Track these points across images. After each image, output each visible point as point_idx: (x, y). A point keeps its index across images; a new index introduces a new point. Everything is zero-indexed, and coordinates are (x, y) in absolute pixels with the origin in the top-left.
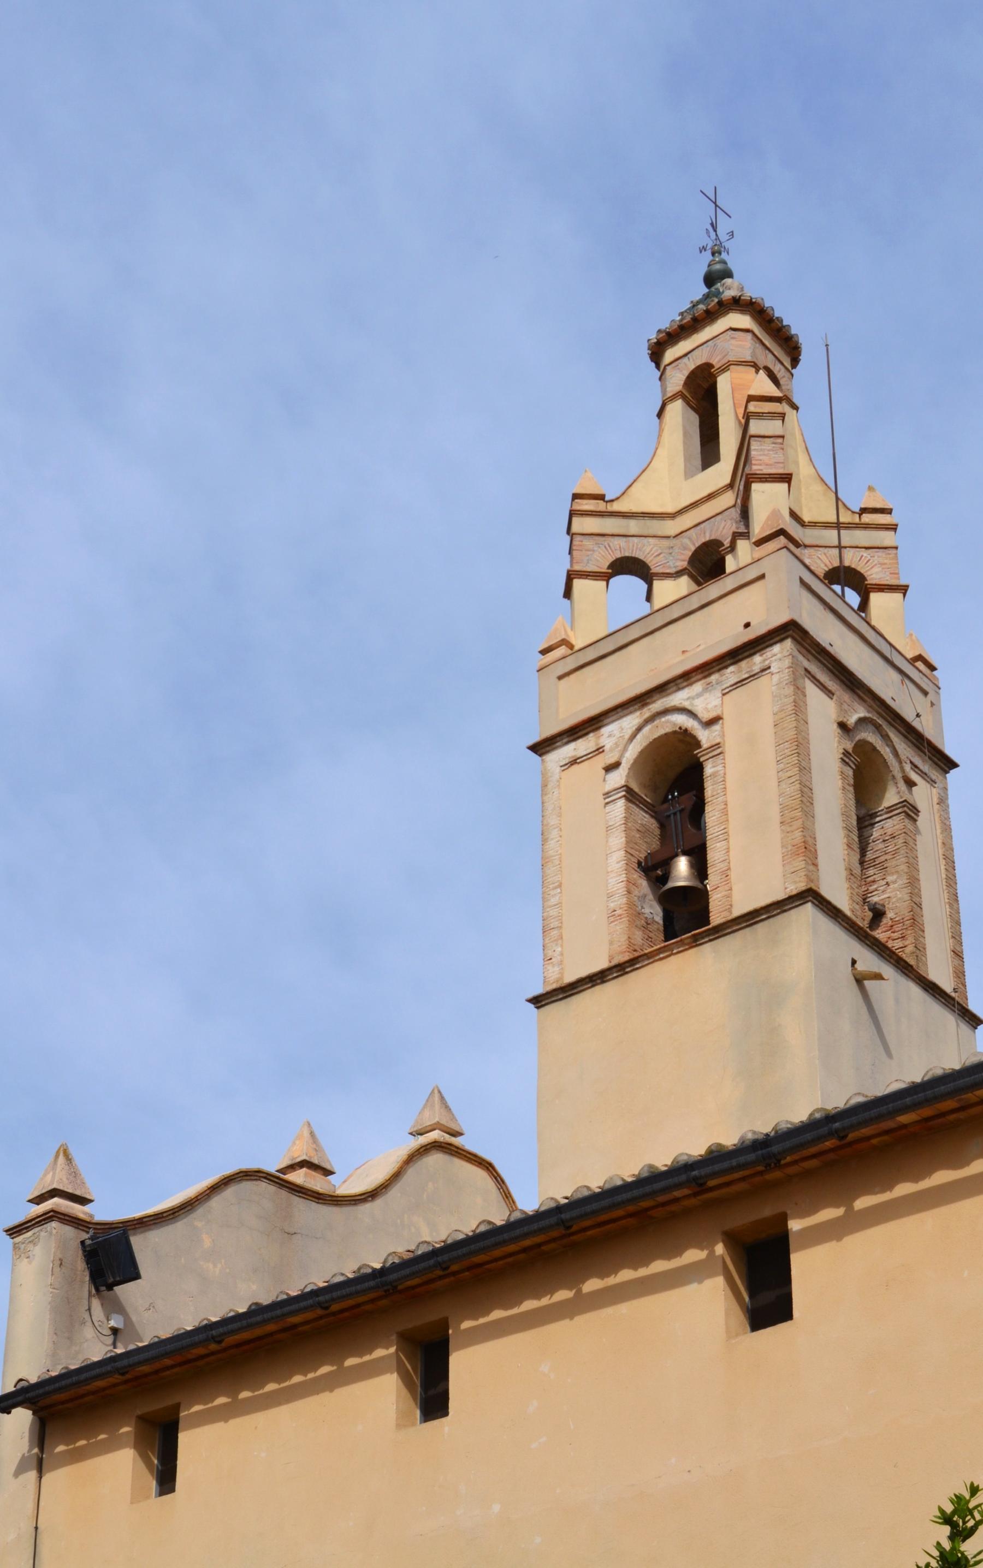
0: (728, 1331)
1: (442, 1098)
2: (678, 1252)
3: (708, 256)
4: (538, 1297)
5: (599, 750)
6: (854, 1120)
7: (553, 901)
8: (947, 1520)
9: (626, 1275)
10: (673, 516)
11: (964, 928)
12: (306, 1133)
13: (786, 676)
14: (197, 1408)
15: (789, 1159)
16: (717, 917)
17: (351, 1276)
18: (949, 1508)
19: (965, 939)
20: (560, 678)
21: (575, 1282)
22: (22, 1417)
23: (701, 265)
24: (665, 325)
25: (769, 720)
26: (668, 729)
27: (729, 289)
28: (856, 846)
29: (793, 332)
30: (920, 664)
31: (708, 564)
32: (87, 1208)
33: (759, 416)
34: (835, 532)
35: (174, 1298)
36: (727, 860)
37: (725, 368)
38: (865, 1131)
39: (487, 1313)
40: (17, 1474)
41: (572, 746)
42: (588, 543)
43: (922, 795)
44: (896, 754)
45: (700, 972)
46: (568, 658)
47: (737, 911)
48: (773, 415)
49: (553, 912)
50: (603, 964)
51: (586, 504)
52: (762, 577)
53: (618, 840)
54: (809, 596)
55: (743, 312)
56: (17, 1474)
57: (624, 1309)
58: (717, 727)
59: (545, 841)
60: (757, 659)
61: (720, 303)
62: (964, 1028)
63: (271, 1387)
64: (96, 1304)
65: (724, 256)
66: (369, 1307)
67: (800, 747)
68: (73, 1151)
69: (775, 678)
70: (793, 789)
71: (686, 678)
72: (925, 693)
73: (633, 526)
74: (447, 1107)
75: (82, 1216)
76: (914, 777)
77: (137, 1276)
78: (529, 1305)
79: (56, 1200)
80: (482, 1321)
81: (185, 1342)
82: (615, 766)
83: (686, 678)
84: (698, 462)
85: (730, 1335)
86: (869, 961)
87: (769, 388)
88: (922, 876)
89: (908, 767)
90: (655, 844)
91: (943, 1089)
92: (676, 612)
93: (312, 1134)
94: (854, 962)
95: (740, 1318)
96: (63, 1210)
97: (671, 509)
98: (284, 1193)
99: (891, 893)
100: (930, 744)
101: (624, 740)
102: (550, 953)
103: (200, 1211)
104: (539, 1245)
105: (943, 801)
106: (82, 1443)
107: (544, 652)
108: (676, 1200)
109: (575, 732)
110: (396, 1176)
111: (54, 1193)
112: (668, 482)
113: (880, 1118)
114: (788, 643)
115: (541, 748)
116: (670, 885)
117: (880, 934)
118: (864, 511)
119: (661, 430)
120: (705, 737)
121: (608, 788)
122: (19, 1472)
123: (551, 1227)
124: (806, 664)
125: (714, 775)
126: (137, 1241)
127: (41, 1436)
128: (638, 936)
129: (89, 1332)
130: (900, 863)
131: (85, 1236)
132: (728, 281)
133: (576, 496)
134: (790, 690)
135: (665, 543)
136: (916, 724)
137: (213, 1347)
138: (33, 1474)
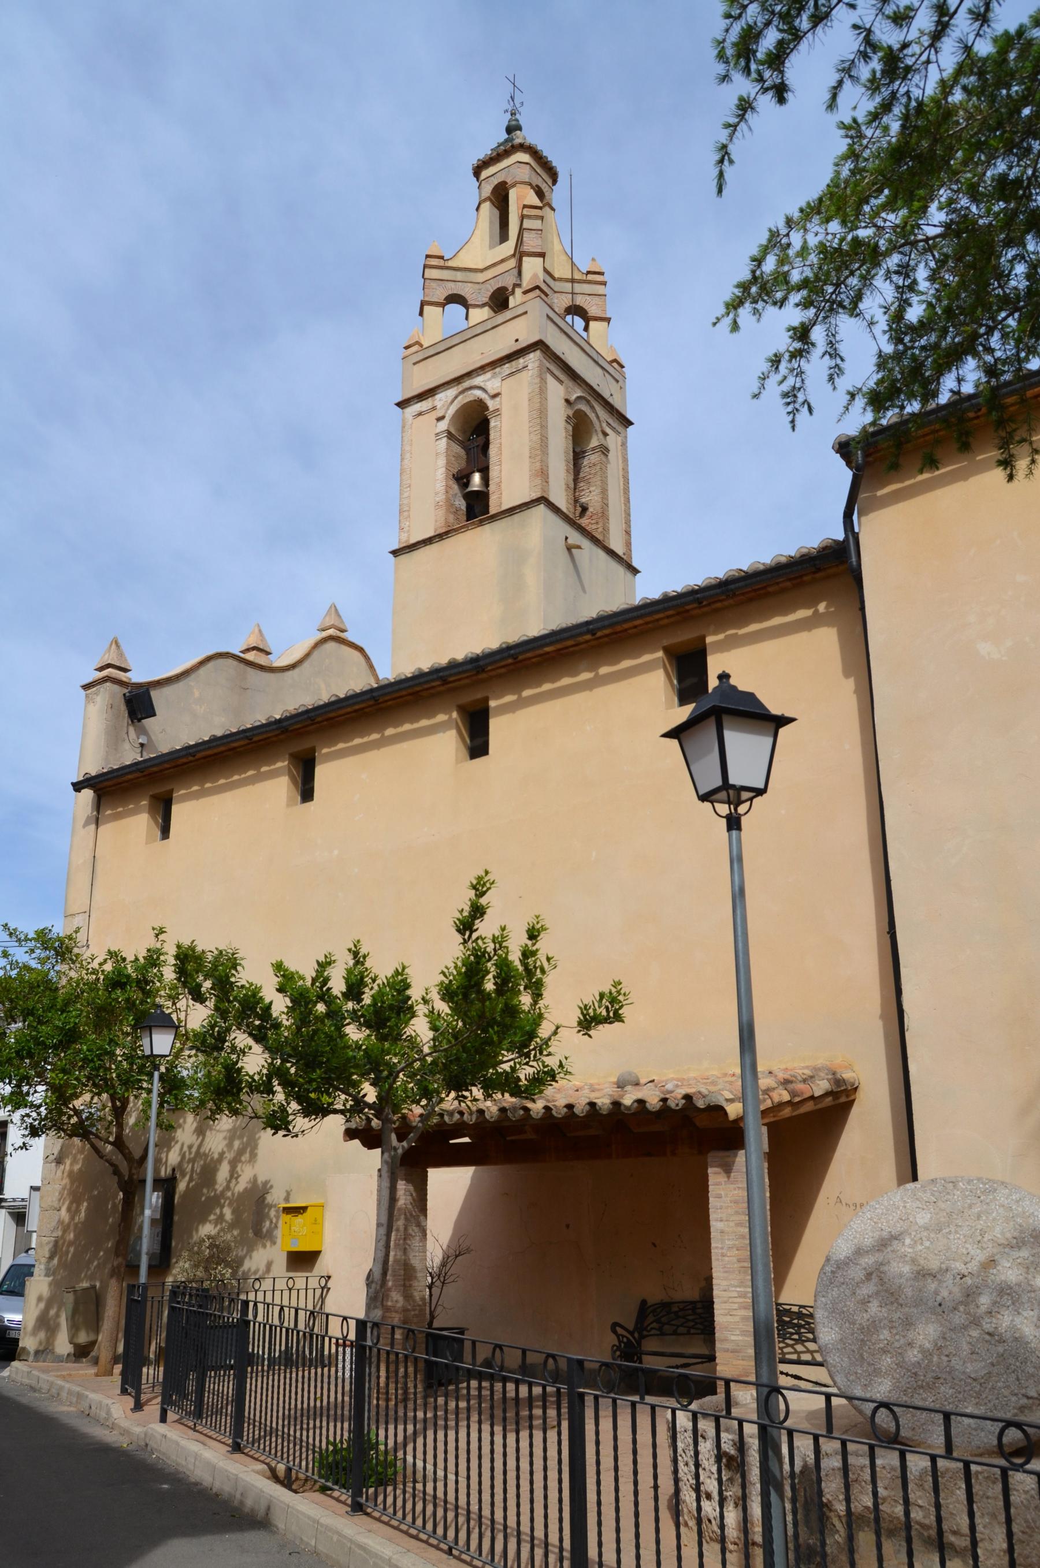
0: (457, 760)
1: (336, 610)
2: (434, 716)
3: (508, 116)
4: (362, 737)
5: (434, 408)
6: (521, 649)
7: (406, 495)
8: (474, 887)
9: (407, 727)
10: (482, 271)
11: (632, 518)
12: (257, 630)
13: (536, 372)
14: (183, 792)
15: (489, 668)
16: (493, 510)
17: (264, 722)
18: (475, 882)
19: (632, 524)
20: (414, 364)
21: (381, 730)
22: (88, 794)
23: (505, 120)
24: (481, 156)
25: (526, 397)
26: (472, 399)
27: (518, 138)
28: (572, 471)
29: (554, 164)
30: (615, 365)
31: (499, 301)
32: (128, 674)
33: (529, 217)
34: (570, 284)
35: (175, 728)
36: (500, 477)
37: (514, 185)
38: (529, 655)
39: (336, 745)
40: (84, 826)
41: (419, 404)
42: (434, 284)
43: (613, 441)
44: (598, 417)
45: (483, 541)
46: (418, 352)
47: (504, 507)
48: (537, 217)
49: (405, 502)
50: (432, 534)
51: (434, 261)
52: (526, 313)
53: (442, 462)
54: (552, 325)
55: (525, 152)
56: (84, 826)
57: (405, 745)
58: (498, 399)
59: (402, 459)
60: (521, 360)
61: (513, 146)
62: (629, 575)
63: (222, 781)
64: (131, 729)
65: (518, 116)
66: (274, 739)
67: (542, 414)
68: (120, 641)
69: (530, 373)
70: (536, 438)
71: (483, 369)
72: (617, 381)
73: (459, 276)
74: (339, 616)
75: (124, 679)
76: (608, 430)
77: (154, 715)
78: (357, 741)
79: (110, 670)
80: (333, 749)
81: (177, 755)
82: (442, 418)
83: (483, 369)
84: (497, 238)
85: (458, 761)
86: (575, 538)
87: (535, 201)
88: (610, 488)
89: (604, 425)
90: (463, 464)
91: (566, 635)
92: (479, 330)
93: (260, 631)
94: (566, 538)
95: (464, 753)
96: (113, 676)
97: (481, 267)
98: (242, 666)
99: (591, 497)
100: (618, 411)
101: (448, 403)
102: (403, 525)
103: (193, 676)
104: (363, 709)
105: (624, 444)
106: (120, 809)
107: (406, 348)
108: (433, 687)
109: (421, 397)
110: (308, 655)
111: (109, 666)
112: (479, 251)
113: (533, 649)
114: (538, 352)
115: (402, 404)
116: (469, 489)
117: (584, 522)
118: (589, 273)
119: (478, 219)
120: (491, 404)
121: (438, 431)
122: (86, 824)
123: (368, 700)
124: (548, 365)
125: (495, 427)
126: (154, 694)
127: (98, 805)
128: (451, 518)
129: (127, 746)
130: (597, 480)
131: (126, 691)
132: (518, 132)
133: (427, 256)
134: (538, 380)
135: (477, 286)
136: (610, 400)
137: (191, 758)
138: (93, 826)
